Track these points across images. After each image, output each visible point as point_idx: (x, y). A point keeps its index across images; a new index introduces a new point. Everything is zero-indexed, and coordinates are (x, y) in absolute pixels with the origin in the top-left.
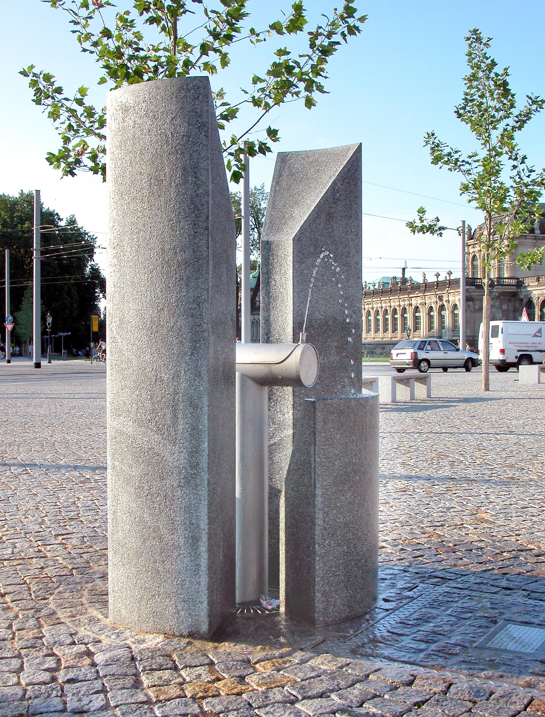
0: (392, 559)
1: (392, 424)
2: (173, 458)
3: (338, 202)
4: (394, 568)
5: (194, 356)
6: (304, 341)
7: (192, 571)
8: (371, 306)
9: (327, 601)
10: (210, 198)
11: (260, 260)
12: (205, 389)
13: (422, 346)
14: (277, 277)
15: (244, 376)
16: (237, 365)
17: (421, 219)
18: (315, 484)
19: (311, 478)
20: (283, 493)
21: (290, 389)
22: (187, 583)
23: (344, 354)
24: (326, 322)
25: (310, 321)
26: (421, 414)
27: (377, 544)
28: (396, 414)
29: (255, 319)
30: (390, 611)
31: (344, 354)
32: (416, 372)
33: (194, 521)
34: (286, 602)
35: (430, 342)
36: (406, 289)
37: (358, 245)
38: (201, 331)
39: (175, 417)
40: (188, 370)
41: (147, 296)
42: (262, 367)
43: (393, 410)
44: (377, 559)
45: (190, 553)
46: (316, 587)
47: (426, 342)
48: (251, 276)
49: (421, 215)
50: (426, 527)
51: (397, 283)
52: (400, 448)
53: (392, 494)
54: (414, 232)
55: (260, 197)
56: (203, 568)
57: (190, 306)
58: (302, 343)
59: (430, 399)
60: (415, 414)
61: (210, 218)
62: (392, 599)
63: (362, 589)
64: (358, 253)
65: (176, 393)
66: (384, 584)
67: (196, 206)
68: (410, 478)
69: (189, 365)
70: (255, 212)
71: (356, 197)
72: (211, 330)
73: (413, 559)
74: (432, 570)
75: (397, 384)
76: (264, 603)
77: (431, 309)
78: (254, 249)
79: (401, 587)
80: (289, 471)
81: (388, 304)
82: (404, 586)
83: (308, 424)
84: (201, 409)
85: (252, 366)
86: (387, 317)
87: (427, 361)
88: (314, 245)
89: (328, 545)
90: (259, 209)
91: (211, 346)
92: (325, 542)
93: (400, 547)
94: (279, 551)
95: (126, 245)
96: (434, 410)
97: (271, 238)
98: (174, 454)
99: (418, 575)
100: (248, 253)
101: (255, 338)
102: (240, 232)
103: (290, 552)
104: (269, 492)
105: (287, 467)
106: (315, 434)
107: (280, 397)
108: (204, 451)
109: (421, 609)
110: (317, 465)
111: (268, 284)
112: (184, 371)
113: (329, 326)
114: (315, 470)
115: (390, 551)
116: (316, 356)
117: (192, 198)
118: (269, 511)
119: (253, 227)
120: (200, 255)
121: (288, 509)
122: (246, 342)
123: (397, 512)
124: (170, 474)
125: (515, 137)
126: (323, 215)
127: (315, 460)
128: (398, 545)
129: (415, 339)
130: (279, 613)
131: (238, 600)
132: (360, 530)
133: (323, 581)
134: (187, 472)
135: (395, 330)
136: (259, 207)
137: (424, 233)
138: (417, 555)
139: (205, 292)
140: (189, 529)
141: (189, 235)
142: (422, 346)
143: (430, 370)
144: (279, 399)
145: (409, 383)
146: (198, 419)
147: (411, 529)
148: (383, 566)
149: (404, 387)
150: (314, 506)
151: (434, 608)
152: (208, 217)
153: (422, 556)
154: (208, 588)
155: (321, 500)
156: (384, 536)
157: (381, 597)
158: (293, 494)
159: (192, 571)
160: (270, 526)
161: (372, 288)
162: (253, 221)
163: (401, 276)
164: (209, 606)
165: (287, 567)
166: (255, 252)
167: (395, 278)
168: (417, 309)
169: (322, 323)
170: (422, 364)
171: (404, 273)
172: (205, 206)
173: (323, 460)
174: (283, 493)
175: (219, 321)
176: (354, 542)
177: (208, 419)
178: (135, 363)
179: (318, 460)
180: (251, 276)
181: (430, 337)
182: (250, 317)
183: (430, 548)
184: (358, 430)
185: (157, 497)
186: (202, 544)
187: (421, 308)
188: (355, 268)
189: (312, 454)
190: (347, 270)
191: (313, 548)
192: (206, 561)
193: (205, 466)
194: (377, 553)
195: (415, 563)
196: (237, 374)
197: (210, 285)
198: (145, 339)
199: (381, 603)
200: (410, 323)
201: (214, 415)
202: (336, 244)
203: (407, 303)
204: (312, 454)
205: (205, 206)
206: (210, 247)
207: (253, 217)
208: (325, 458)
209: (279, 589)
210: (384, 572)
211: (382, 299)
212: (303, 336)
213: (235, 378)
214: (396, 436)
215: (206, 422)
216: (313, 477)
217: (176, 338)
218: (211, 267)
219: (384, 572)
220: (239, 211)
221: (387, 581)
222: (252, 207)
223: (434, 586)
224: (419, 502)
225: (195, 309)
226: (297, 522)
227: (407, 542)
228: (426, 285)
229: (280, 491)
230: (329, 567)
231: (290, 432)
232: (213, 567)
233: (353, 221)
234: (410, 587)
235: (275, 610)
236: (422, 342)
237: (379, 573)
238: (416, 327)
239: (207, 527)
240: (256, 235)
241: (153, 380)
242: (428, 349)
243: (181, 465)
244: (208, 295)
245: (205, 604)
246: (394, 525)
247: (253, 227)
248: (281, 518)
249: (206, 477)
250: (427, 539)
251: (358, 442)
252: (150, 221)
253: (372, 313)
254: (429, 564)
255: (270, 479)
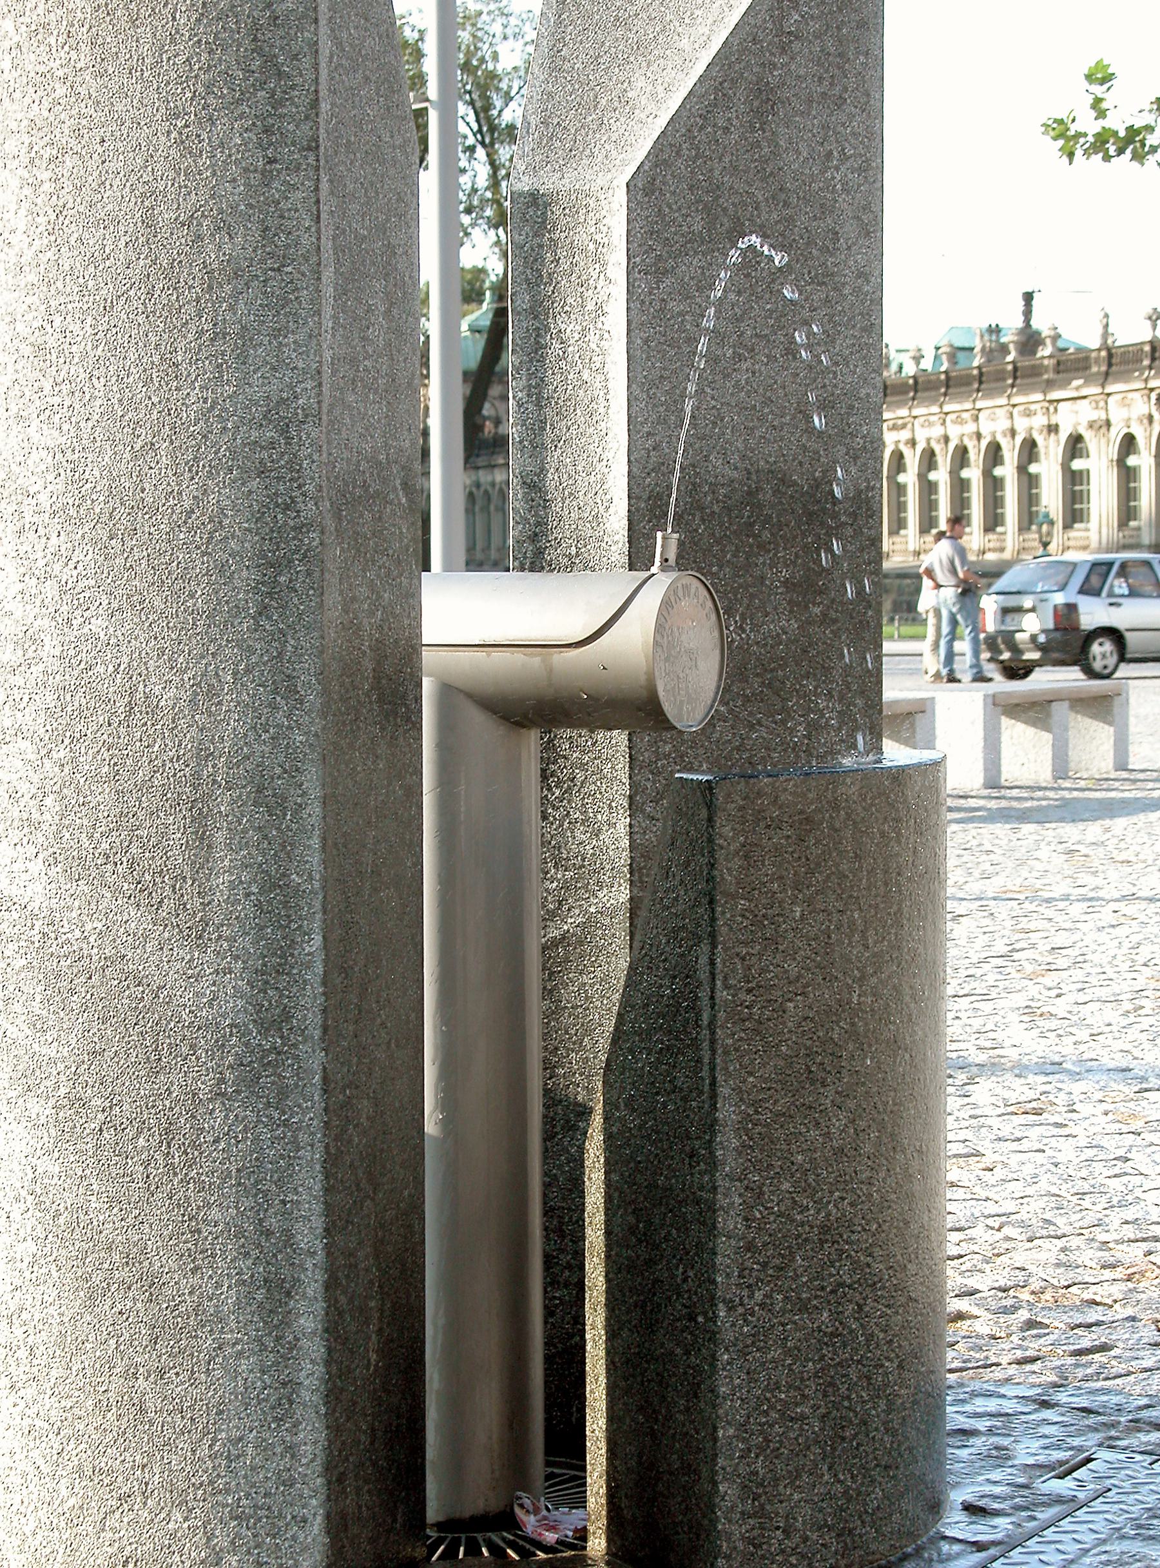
0: (993, 1360)
1: (987, 866)
2: (197, 994)
3: (797, 45)
4: (1002, 1391)
5: (269, 618)
6: (672, 556)
7: (265, 1406)
8: (905, 435)
9: (760, 1513)
10: (324, 30)
11: (495, 267)
12: (312, 740)
13: (1095, 581)
14: (571, 329)
15: (448, 691)
16: (426, 654)
17: (1098, 108)
18: (713, 1083)
19: (699, 1061)
20: (597, 1120)
21: (620, 738)
22: (250, 1450)
23: (817, 610)
24: (749, 493)
25: (691, 487)
26: (1094, 830)
27: (943, 1304)
28: (1001, 829)
29: (478, 485)
30: (993, 1551)
31: (817, 610)
32: (1070, 677)
33: (273, 1222)
34: (610, 1518)
35: (1124, 566)
36: (1035, 371)
37: (867, 208)
38: (294, 528)
39: (202, 839)
40: (248, 671)
41: (93, 398)
42: (517, 658)
43: (993, 817)
44: (942, 1359)
45: (259, 1340)
46: (721, 1462)
47: (1110, 564)
48: (464, 326)
49: (1098, 90)
50: (1117, 1242)
51: (1004, 349)
52: (1016, 956)
53: (989, 1121)
54: (1071, 155)
55: (496, 28)
56: (306, 1395)
57: (255, 434)
58: (664, 568)
59: (1125, 775)
60: (1070, 832)
61: (324, 107)
62: (996, 1506)
63: (887, 1467)
64: (868, 233)
65: (204, 755)
66: (966, 1451)
67: (270, 60)
68: (1052, 1068)
69: (251, 651)
70: (476, 84)
71: (862, 25)
72: (330, 524)
73: (1071, 1361)
74: (1144, 1401)
75: (1005, 721)
76: (530, 1523)
77: (1129, 444)
78: (473, 225)
79: (1031, 1461)
80: (617, 1038)
81: (971, 427)
82: (1041, 1459)
83: (687, 864)
84: (295, 813)
85: (481, 654)
86: (965, 474)
87: (1114, 634)
88: (707, 208)
89: (762, 1305)
90: (493, 76)
91: (333, 579)
92: (751, 1297)
93: (1023, 1315)
94: (583, 1332)
95: (13, 207)
96: (1142, 816)
97: (548, 182)
98: (198, 977)
99: (1092, 1420)
100: (452, 237)
101: (479, 556)
102: (422, 160)
103: (625, 1333)
104: (545, 1116)
105: (610, 1025)
106: (711, 902)
107: (583, 767)
108: (308, 966)
109: (1104, 1542)
110: (722, 1015)
111: (536, 351)
112: (235, 674)
113: (760, 506)
114: (713, 1033)
115: (985, 1330)
116: (714, 617)
117: (256, 28)
118: (546, 1186)
119: (471, 141)
120: (287, 246)
121: (615, 1177)
122: (448, 567)
123: (1012, 1186)
124: (185, 1050)
125: (425, 52)
126: (741, 94)
127: (712, 998)
128: (1014, 1309)
129: (1072, 556)
130: (584, 1558)
131: (433, 1512)
132: (877, 1252)
133: (744, 1440)
134: (247, 1044)
135: (993, 521)
136: (490, 67)
137: (1107, 158)
138: (1086, 1343)
139: (309, 384)
140: (255, 1253)
141: (246, 170)
142: (1095, 581)
143: (1124, 670)
144: (580, 776)
145: (1049, 715)
146: (286, 848)
147: (1064, 1250)
148: (962, 1385)
149: (1030, 731)
150: (713, 1165)
151: (1152, 1538)
152: (315, 104)
153: (1104, 1348)
154: (328, 1468)
155: (735, 1143)
156: (962, 1273)
157: (958, 1497)
158: (633, 1122)
159: (265, 1406)
160: (547, 1238)
161: (910, 369)
162: (471, 118)
163: (1019, 323)
164: (328, 1533)
165: (611, 1389)
166: (476, 233)
167: (995, 330)
168: (1075, 447)
169: (737, 496)
170: (1096, 649)
171: (1028, 313)
172: (306, 62)
173: (742, 996)
174: (597, 1120)
175: (358, 492)
176: (857, 1297)
177: (324, 848)
178: (51, 647)
179: (723, 995)
180: (464, 326)
181: (1126, 547)
182: (463, 479)
183: (1133, 1319)
184: (868, 889)
185: (137, 1137)
186: (302, 1306)
187: (1091, 440)
188: (857, 291)
189: (703, 975)
190: (827, 300)
191: (707, 1319)
192: (320, 1370)
193: (313, 1020)
194: (942, 1336)
195: (1080, 1372)
196: (427, 684)
197: (327, 355)
198: (87, 557)
199: (956, 1525)
200: (1051, 497)
201: (345, 835)
202: (786, 204)
203: (1040, 421)
204: (703, 975)
205: (306, 62)
206: (323, 216)
207: (472, 103)
208: (749, 991)
209: (584, 1469)
210: (968, 1408)
211: (946, 408)
212: (665, 543)
213: (418, 699)
214: (1003, 910)
215: (315, 860)
216: (706, 1060)
217: (204, 554)
218: (329, 291)
219: (968, 1408)
220: (420, 80)
221: (978, 1441)
222: (466, 67)
223: (1149, 1459)
224: (1090, 1153)
225: (272, 445)
226: (649, 1223)
227: (1048, 1296)
228: (1110, 355)
229: (584, 1112)
230: (766, 1389)
231: (621, 894)
232: (342, 1390)
233: (851, 117)
234: (1061, 1463)
235: (572, 1547)
236: (1095, 565)
237: (949, 1409)
238: (1074, 514)
239: (319, 1245)
240: (483, 172)
241: (121, 703)
242: (1117, 591)
243: (224, 1016)
244: (319, 394)
245: (317, 1525)
246: (999, 1235)
247: (471, 141)
248: (589, 1208)
249: (315, 1060)
250: (1123, 1286)
251: (871, 932)
252: (99, 117)
253: (912, 461)
254: (1132, 1378)
255: (549, 1067)
